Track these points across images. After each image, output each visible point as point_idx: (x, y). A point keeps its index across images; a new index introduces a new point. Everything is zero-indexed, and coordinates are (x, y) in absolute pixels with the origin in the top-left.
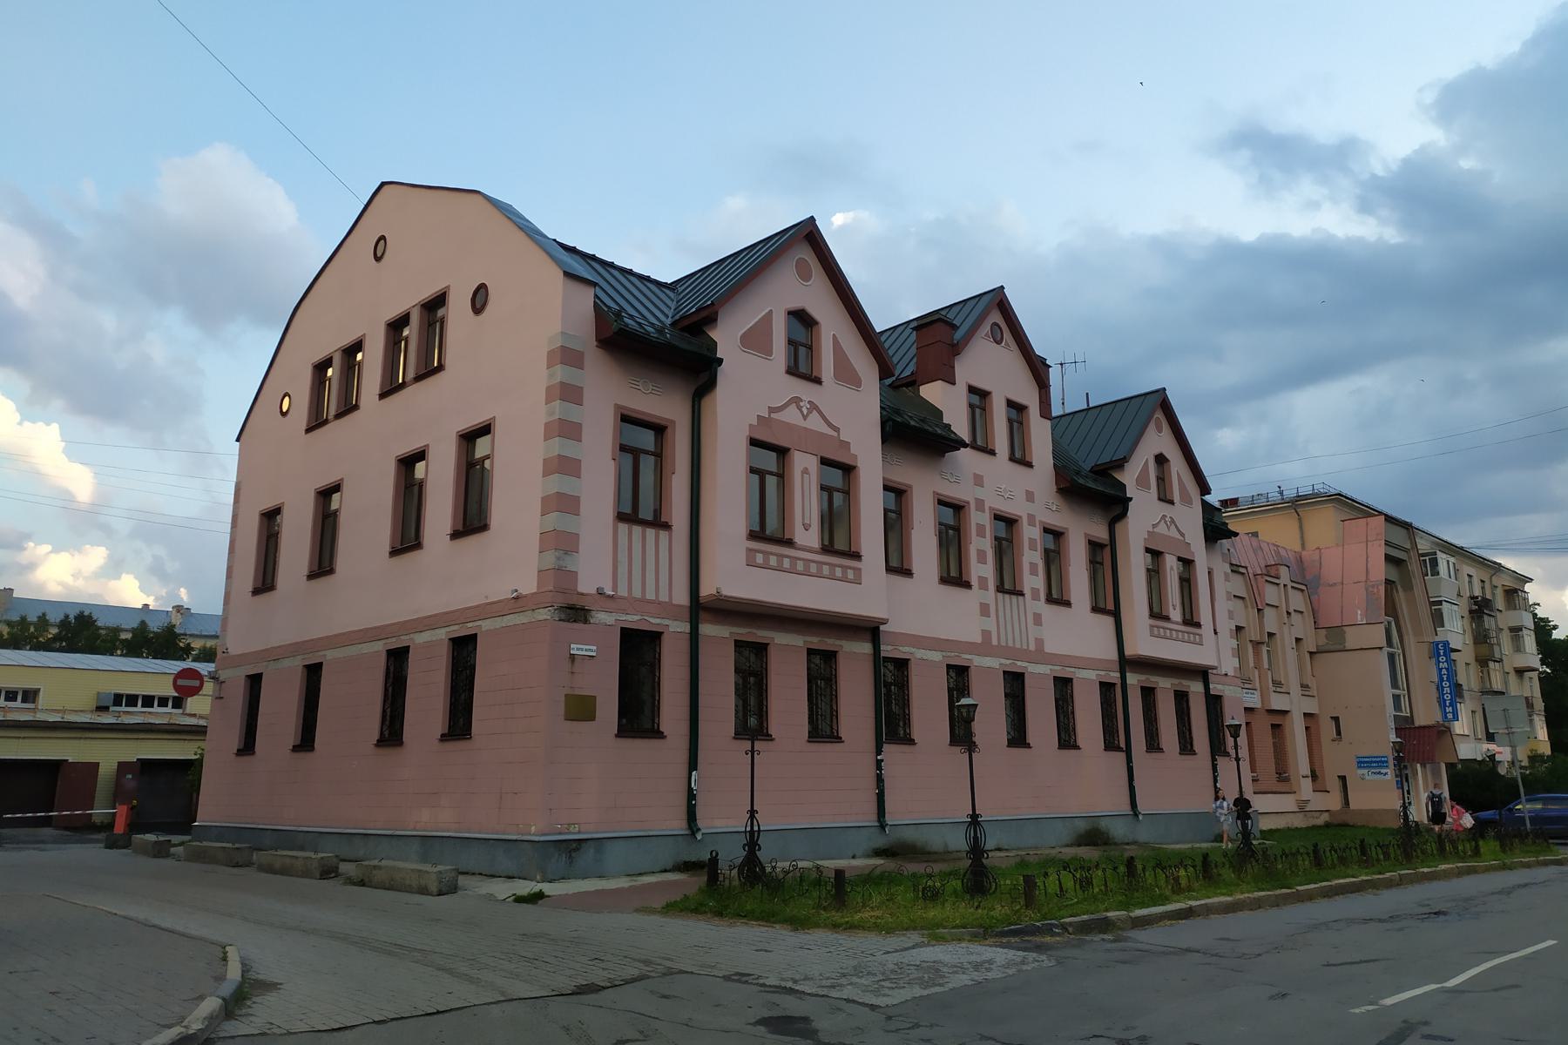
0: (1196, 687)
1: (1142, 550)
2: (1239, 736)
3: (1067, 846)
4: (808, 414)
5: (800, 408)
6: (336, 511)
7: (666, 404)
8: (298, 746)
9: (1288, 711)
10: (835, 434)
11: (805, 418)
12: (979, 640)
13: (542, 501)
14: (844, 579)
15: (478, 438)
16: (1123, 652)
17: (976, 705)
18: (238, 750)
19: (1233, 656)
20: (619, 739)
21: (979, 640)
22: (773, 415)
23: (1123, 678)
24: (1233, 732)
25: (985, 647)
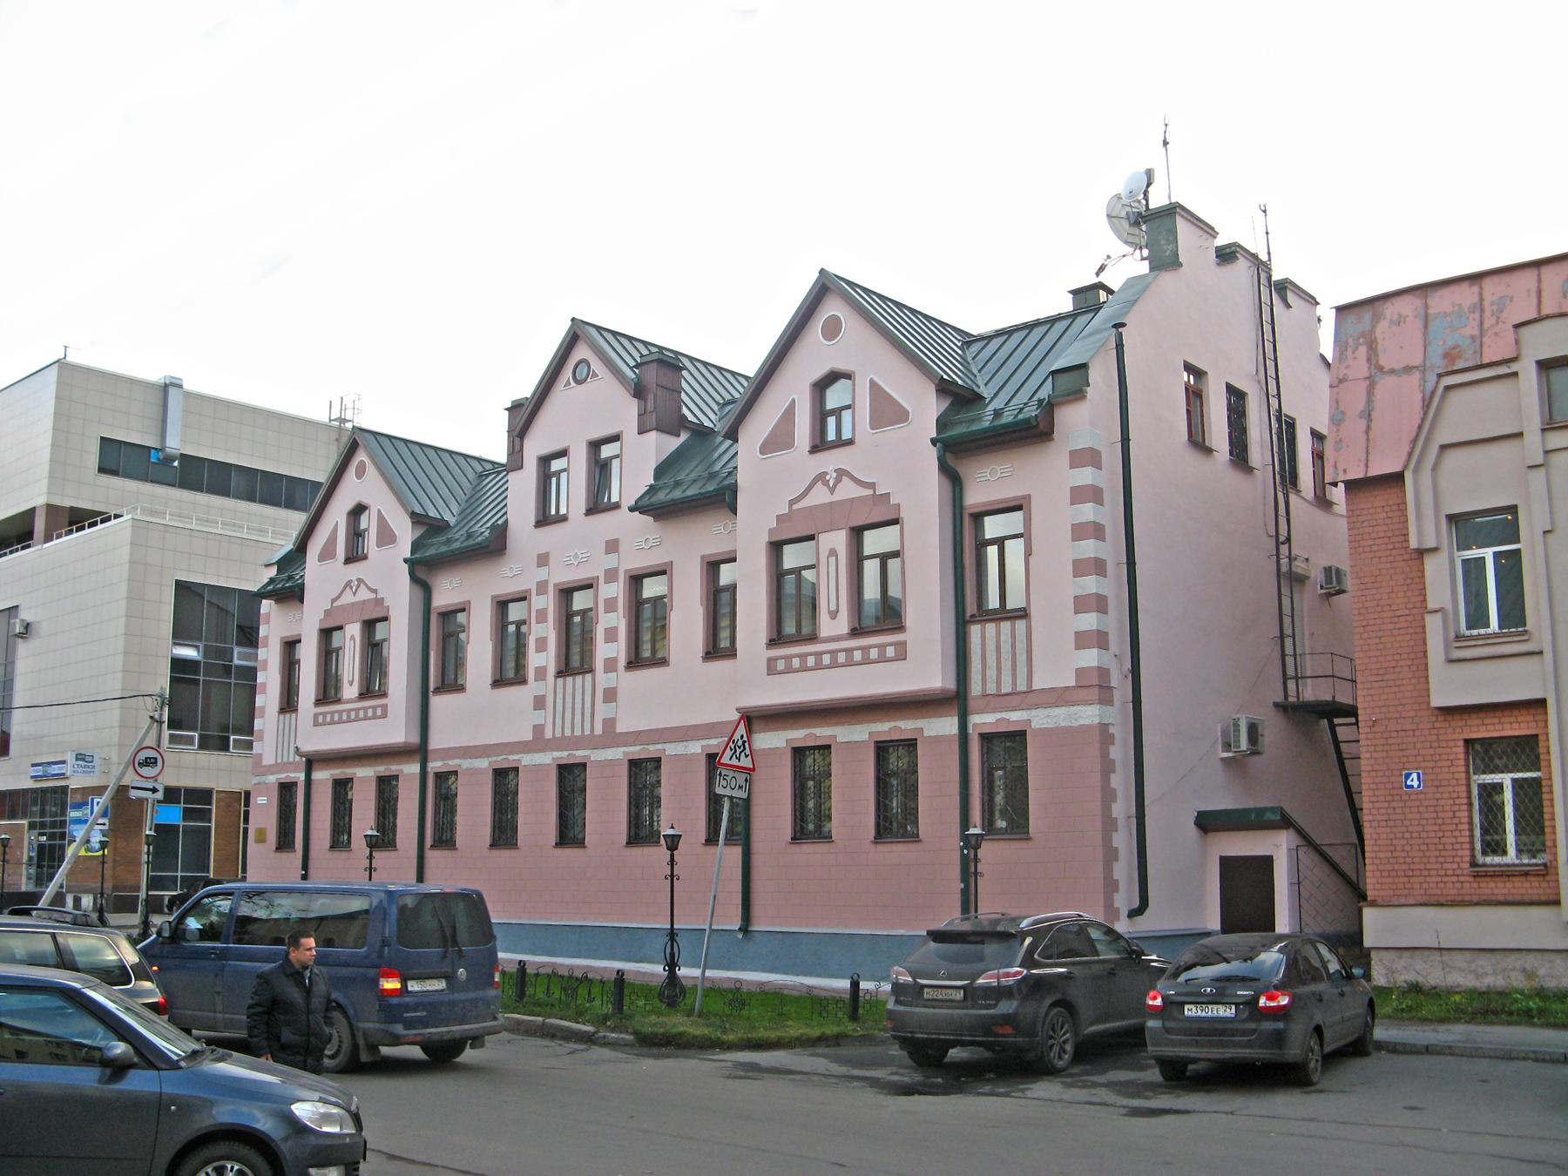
0: (412, 769)
1: (1105, 216)
2: (677, 849)
3: (366, 1039)
4: (835, 485)
5: (826, 483)
6: (365, 530)
8: (438, 688)
9: (17, 606)
10: (870, 492)
11: (832, 490)
12: (528, 736)
13: (1118, 857)
14: (375, 717)
15: (1109, 783)
16: (722, 563)
17: (680, 836)
18: (556, 844)
19: (513, 402)
20: (347, 566)
21: (528, 736)
22: (795, 507)
24: (669, 843)
25: (539, 741)
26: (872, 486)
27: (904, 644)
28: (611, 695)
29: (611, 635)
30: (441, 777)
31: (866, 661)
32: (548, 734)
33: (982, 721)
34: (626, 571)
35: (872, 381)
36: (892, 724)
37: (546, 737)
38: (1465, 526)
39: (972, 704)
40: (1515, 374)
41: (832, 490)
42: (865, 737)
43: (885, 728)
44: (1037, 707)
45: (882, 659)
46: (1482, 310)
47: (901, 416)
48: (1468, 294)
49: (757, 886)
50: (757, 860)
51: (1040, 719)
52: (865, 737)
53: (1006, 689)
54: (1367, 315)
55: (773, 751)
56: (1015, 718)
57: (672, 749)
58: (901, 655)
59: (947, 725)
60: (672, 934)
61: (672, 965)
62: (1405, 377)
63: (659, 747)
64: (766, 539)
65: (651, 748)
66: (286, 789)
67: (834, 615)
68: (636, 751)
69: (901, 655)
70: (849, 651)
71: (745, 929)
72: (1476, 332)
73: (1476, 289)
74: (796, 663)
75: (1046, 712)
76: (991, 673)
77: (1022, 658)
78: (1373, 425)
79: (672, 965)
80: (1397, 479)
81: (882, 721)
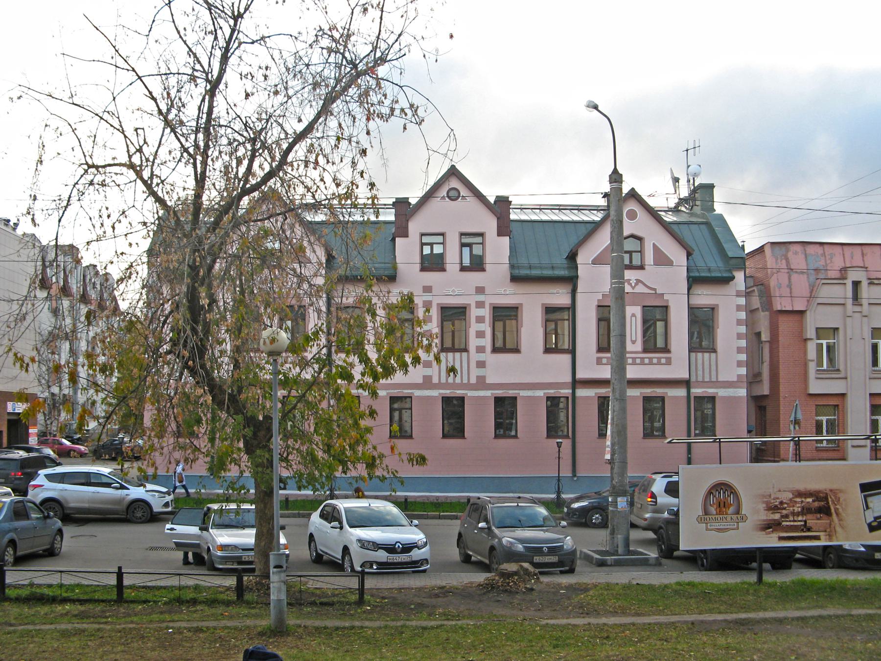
7: (559, 297)
12: (420, 381)
23: (574, 393)
26: (655, 290)
27: (670, 358)
28: (481, 364)
29: (480, 334)
30: (699, 399)
31: (651, 363)
32: (435, 380)
33: (696, 391)
34: (438, 304)
35: (654, 244)
36: (652, 390)
37: (487, 382)
38: (821, 332)
39: (692, 384)
40: (845, 284)
41: (633, 288)
42: (638, 394)
43: (648, 391)
44: (721, 387)
45: (659, 363)
46: (825, 257)
47: (669, 263)
48: (819, 249)
49: (578, 457)
50: (579, 446)
51: (722, 393)
52: (638, 394)
53: (707, 379)
54: (783, 248)
55: (633, 398)
56: (711, 391)
57: (523, 393)
58: (669, 362)
59: (681, 392)
60: (559, 479)
61: (559, 493)
62: (801, 275)
63: (516, 391)
64: (596, 303)
65: (511, 392)
66: (553, 402)
67: (634, 342)
68: (500, 393)
69: (669, 362)
70: (642, 359)
71: (574, 476)
72: (824, 264)
73: (822, 248)
74: (655, 361)
75: (724, 390)
76: (700, 373)
77: (713, 368)
78: (793, 291)
79: (559, 493)
80: (802, 313)
81: (635, 390)
